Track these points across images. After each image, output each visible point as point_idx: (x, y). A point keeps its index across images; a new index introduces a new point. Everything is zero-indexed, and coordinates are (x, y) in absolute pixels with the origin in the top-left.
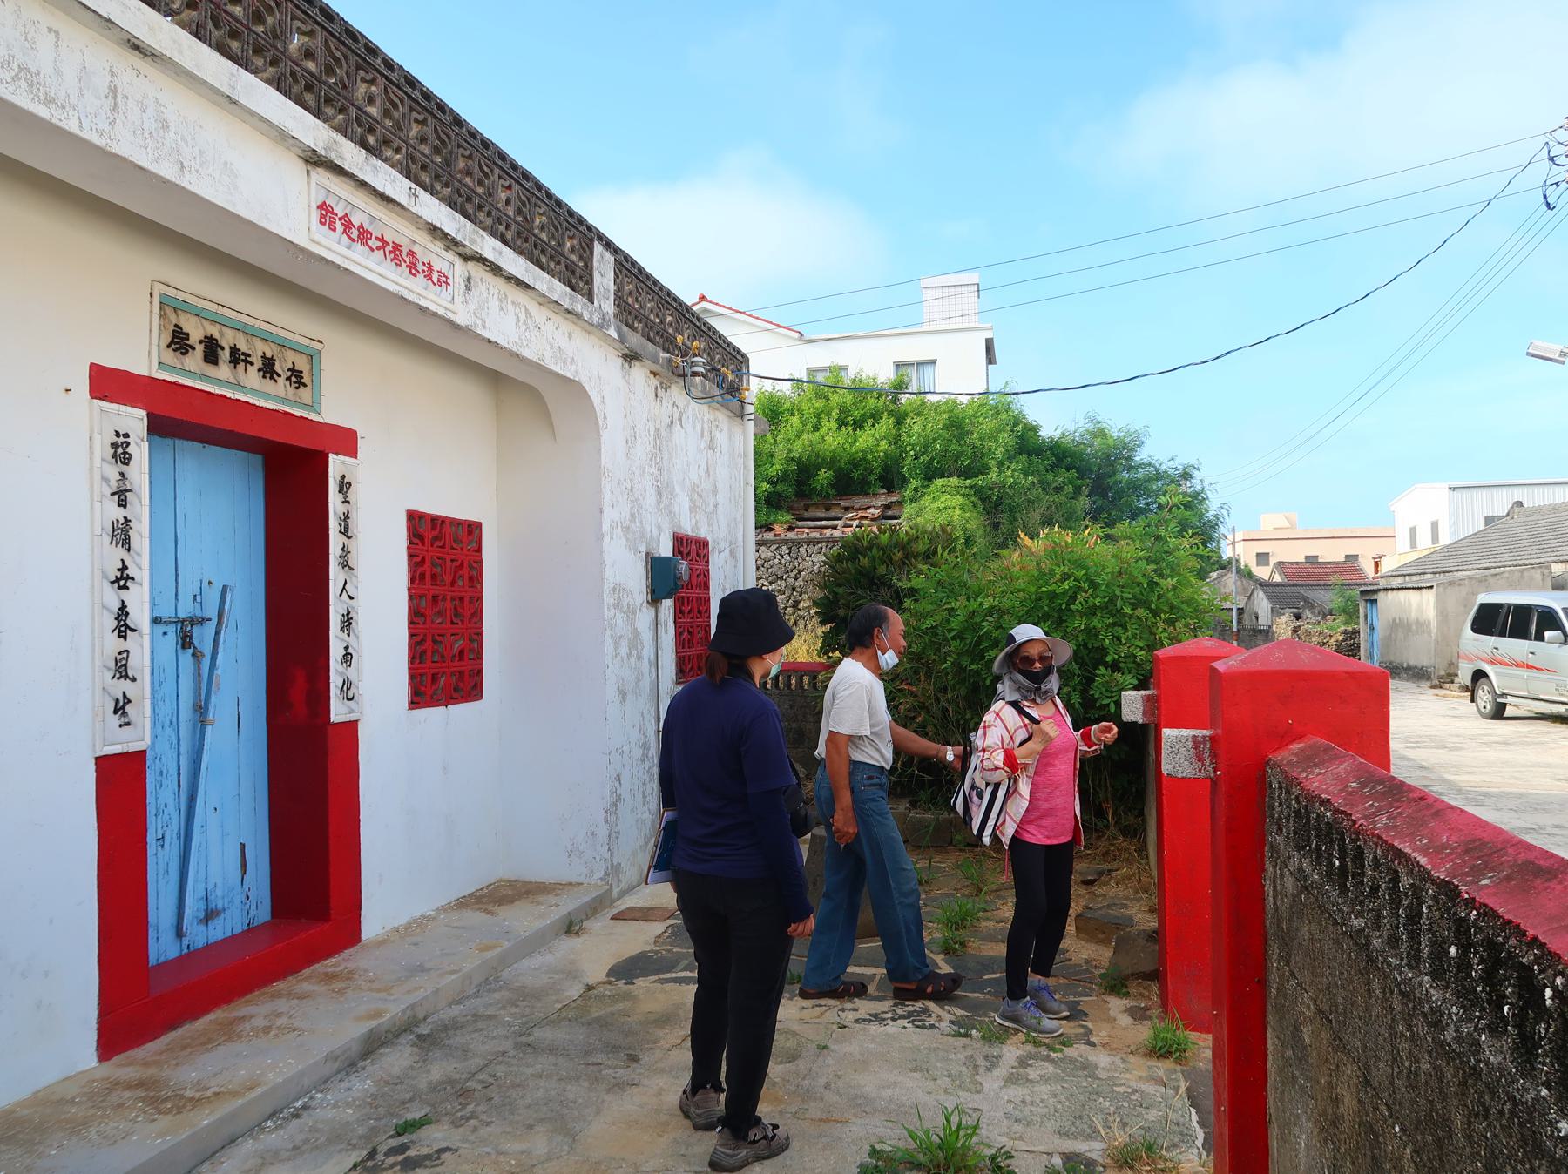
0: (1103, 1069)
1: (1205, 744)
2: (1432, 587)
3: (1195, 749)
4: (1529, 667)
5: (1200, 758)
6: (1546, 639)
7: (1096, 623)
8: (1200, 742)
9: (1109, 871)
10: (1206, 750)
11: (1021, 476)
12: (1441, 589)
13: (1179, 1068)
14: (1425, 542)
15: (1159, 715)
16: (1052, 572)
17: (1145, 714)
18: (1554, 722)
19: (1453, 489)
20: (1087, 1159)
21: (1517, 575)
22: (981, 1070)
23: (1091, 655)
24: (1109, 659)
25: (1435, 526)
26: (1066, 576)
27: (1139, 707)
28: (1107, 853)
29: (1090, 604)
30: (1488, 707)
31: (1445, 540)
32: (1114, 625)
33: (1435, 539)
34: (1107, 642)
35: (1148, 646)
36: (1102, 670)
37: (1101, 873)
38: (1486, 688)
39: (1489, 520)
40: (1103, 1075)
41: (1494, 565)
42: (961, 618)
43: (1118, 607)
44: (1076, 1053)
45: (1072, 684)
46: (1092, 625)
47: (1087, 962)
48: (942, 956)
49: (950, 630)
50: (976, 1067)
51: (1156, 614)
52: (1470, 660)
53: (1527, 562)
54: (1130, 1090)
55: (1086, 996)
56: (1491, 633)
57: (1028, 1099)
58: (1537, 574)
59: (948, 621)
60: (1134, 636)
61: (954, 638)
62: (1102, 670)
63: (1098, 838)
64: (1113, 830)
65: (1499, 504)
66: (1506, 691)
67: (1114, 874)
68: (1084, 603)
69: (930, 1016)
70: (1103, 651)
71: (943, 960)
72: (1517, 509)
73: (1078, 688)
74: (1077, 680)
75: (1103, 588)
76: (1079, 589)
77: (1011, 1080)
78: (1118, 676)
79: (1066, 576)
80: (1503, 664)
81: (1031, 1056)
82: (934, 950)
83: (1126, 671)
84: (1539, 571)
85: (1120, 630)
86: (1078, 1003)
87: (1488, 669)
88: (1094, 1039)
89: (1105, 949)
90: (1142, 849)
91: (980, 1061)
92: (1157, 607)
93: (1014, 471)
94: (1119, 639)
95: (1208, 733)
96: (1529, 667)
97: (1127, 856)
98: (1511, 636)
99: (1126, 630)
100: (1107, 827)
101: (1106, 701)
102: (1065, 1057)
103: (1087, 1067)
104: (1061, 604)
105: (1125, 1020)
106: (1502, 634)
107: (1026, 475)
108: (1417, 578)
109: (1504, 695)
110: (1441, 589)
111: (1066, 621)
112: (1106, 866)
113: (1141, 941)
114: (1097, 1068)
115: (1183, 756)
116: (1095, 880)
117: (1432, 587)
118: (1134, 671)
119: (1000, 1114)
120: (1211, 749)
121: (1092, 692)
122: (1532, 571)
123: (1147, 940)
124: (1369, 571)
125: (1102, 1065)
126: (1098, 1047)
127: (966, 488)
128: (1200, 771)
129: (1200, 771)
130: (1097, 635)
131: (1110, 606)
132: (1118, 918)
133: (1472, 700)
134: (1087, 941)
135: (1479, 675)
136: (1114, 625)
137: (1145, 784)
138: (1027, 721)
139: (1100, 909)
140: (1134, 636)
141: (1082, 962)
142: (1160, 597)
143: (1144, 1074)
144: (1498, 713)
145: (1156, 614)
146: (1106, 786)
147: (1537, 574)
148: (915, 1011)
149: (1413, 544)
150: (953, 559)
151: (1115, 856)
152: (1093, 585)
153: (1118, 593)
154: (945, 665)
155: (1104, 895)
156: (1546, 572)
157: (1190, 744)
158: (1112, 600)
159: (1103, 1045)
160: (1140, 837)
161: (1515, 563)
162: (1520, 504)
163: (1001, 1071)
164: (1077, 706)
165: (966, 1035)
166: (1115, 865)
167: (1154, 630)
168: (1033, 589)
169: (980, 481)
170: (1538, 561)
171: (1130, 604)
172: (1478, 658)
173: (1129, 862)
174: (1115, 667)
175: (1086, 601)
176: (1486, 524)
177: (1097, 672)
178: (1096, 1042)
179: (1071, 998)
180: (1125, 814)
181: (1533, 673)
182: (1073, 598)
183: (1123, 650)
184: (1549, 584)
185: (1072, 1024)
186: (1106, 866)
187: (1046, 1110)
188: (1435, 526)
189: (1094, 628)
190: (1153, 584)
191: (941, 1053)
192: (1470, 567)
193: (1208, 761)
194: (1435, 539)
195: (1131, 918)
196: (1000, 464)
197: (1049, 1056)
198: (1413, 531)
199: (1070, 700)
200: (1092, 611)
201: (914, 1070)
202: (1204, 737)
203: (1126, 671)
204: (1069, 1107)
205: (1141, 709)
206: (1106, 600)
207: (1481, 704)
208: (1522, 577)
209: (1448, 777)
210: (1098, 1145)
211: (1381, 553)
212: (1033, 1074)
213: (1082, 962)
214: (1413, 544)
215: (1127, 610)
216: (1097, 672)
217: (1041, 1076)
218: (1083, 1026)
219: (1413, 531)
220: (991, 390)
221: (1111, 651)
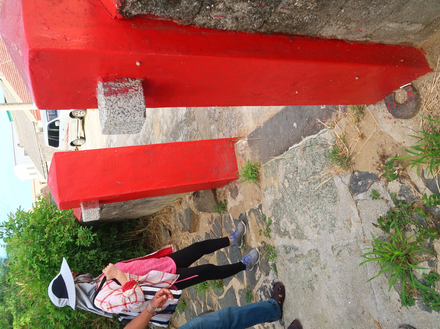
0: (275, 196)
1: (111, 86)
2: (46, 162)
3: (117, 94)
4: (68, 130)
5: (125, 90)
6: (58, 126)
7: (54, 250)
8: (110, 90)
9: (164, 226)
10: (117, 85)
11: (12, 297)
12: (47, 160)
13: (263, 165)
14: (35, 171)
15: (94, 199)
16: (30, 275)
17: (94, 207)
18: (84, 124)
19: (16, 164)
20: (351, 182)
21: (40, 141)
22: (298, 253)
23: (71, 249)
24: (71, 240)
25: (28, 168)
26: (31, 268)
27: (91, 210)
28: (156, 229)
29: (44, 254)
30: (82, 141)
31: (33, 165)
32: (54, 242)
33: (33, 168)
34: (63, 242)
35: (64, 225)
36: (78, 243)
37: (166, 229)
38: (76, 142)
39: (26, 154)
40: (279, 196)
41: (38, 148)
42: (59, 315)
43: (45, 240)
44: (269, 211)
45: (86, 255)
46: (56, 251)
47: (210, 223)
48: (224, 287)
49: (66, 319)
50: (296, 256)
51: (47, 223)
52: (68, 147)
53: (36, 139)
54: (286, 180)
55: (230, 218)
56: (58, 142)
57: (312, 224)
58: (39, 136)
59: (62, 321)
60: (59, 231)
61: (70, 316)
62: (78, 243)
63: (150, 234)
64: (146, 228)
65: (20, 151)
66: (76, 137)
67: (165, 224)
68: (44, 257)
69: (266, 286)
70: (68, 244)
71: (227, 286)
72: (20, 145)
73: (87, 252)
74: (84, 253)
75: (35, 249)
76: (37, 261)
77: (300, 235)
78: (79, 235)
79: (31, 268)
80: (68, 137)
81: (278, 231)
82: (221, 291)
83: (77, 232)
84: (39, 135)
85: (57, 238)
86: (235, 220)
87: (70, 142)
88: (257, 206)
89: (201, 218)
90: (153, 216)
91: (292, 254)
92: (44, 223)
93: (9, 301)
94: (62, 238)
95: (100, 85)
96: (68, 130)
97: (156, 221)
98: (59, 136)
99: (57, 235)
100: (145, 231)
101: (92, 239)
102: (273, 215)
103: (276, 204)
104: (46, 268)
105: (240, 197)
106: (58, 138)
107: (11, 296)
108: (44, 169)
109: (78, 137)
110: (47, 160)
111: (55, 264)
112: (162, 228)
113: (200, 199)
114: (275, 199)
115: (126, 104)
116: (169, 231)
117: (46, 162)
118: (76, 229)
119: (332, 236)
120: (115, 81)
121: (89, 246)
122: (39, 137)
123: (199, 197)
124: (45, 185)
125: (273, 198)
126: (261, 203)
127: (17, 318)
128: (136, 90)
129: (136, 90)
130: (61, 248)
131: (45, 244)
132: (187, 215)
133: (80, 146)
134: (199, 226)
135: (72, 144)
136: (54, 242)
137: (125, 219)
138: (105, 283)
139: (183, 224)
140: (59, 231)
141: (211, 225)
142: (39, 224)
143: (272, 178)
144: (84, 138)
145: (47, 223)
146: (129, 234)
147: (39, 136)
148: (264, 294)
149: (35, 174)
150: (28, 326)
151: (157, 226)
152: (34, 254)
153: (37, 242)
154: (84, 317)
155: (175, 225)
156: (39, 133)
157: (113, 98)
158: (43, 244)
159: (259, 201)
160: (147, 218)
161: (37, 142)
162: (19, 144)
163: (296, 243)
164: (96, 251)
165: (274, 266)
166: (161, 225)
167: (55, 223)
168: (39, 283)
169: (14, 313)
170: (36, 136)
171: (43, 235)
172: (67, 145)
173: (158, 219)
174: (75, 237)
175: (44, 256)
176: (27, 155)
177: (78, 244)
178: (258, 205)
179: (233, 224)
180: (139, 225)
181: (69, 129)
182: (43, 262)
183: (67, 235)
184: (42, 133)
185: (249, 219)
186: (162, 228)
187: (319, 214)
188: (28, 168)
189: (57, 250)
190: (33, 227)
191: (293, 276)
192: (39, 154)
193: (126, 84)
194: (33, 168)
195: (186, 211)
196: (7, 306)
197: (275, 223)
198: (31, 174)
199: (94, 255)
200: (49, 253)
201: (313, 289)
202: (104, 86)
203: (77, 232)
204: (312, 202)
205: (92, 209)
206: (42, 247)
207: (81, 143)
208: (41, 139)
209: (105, 142)
210: (337, 181)
211: (39, 182)
212: (291, 227)
213: (211, 225)
214: (35, 174)
215: (46, 236)
216: (78, 244)
217: (291, 223)
218: (249, 214)
219: (31, 174)
220: (107, 286)
221: (67, 240)
